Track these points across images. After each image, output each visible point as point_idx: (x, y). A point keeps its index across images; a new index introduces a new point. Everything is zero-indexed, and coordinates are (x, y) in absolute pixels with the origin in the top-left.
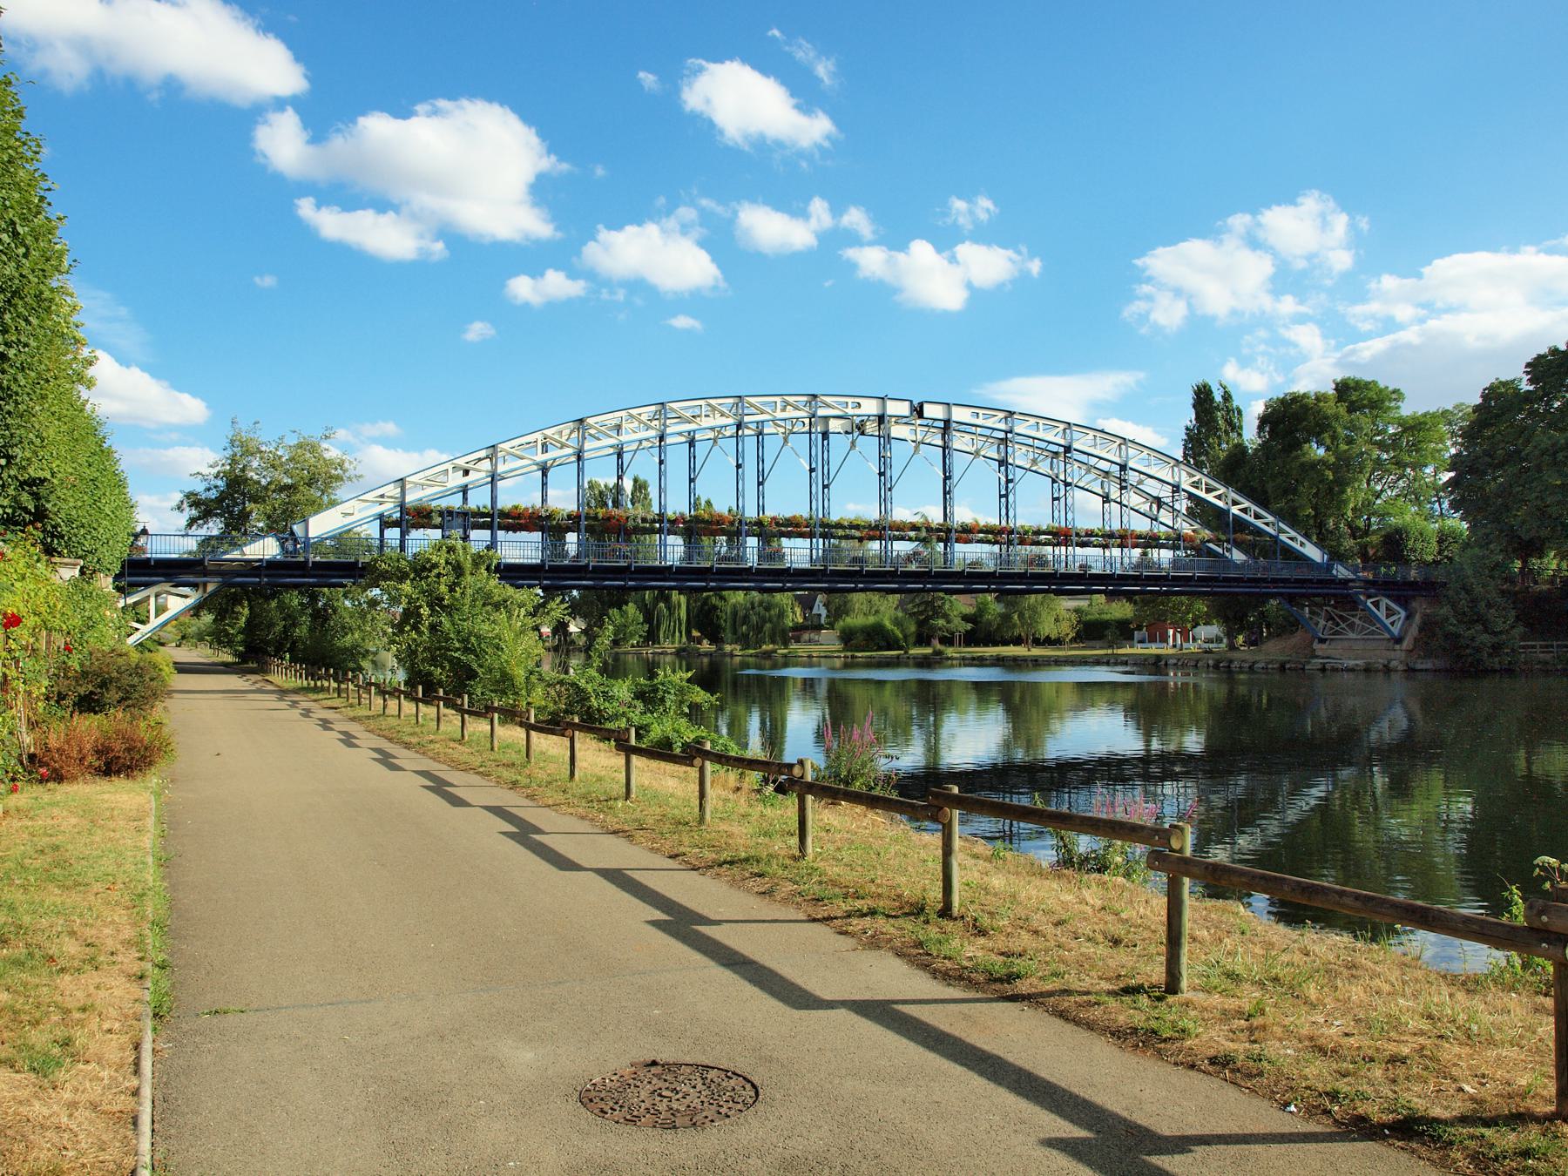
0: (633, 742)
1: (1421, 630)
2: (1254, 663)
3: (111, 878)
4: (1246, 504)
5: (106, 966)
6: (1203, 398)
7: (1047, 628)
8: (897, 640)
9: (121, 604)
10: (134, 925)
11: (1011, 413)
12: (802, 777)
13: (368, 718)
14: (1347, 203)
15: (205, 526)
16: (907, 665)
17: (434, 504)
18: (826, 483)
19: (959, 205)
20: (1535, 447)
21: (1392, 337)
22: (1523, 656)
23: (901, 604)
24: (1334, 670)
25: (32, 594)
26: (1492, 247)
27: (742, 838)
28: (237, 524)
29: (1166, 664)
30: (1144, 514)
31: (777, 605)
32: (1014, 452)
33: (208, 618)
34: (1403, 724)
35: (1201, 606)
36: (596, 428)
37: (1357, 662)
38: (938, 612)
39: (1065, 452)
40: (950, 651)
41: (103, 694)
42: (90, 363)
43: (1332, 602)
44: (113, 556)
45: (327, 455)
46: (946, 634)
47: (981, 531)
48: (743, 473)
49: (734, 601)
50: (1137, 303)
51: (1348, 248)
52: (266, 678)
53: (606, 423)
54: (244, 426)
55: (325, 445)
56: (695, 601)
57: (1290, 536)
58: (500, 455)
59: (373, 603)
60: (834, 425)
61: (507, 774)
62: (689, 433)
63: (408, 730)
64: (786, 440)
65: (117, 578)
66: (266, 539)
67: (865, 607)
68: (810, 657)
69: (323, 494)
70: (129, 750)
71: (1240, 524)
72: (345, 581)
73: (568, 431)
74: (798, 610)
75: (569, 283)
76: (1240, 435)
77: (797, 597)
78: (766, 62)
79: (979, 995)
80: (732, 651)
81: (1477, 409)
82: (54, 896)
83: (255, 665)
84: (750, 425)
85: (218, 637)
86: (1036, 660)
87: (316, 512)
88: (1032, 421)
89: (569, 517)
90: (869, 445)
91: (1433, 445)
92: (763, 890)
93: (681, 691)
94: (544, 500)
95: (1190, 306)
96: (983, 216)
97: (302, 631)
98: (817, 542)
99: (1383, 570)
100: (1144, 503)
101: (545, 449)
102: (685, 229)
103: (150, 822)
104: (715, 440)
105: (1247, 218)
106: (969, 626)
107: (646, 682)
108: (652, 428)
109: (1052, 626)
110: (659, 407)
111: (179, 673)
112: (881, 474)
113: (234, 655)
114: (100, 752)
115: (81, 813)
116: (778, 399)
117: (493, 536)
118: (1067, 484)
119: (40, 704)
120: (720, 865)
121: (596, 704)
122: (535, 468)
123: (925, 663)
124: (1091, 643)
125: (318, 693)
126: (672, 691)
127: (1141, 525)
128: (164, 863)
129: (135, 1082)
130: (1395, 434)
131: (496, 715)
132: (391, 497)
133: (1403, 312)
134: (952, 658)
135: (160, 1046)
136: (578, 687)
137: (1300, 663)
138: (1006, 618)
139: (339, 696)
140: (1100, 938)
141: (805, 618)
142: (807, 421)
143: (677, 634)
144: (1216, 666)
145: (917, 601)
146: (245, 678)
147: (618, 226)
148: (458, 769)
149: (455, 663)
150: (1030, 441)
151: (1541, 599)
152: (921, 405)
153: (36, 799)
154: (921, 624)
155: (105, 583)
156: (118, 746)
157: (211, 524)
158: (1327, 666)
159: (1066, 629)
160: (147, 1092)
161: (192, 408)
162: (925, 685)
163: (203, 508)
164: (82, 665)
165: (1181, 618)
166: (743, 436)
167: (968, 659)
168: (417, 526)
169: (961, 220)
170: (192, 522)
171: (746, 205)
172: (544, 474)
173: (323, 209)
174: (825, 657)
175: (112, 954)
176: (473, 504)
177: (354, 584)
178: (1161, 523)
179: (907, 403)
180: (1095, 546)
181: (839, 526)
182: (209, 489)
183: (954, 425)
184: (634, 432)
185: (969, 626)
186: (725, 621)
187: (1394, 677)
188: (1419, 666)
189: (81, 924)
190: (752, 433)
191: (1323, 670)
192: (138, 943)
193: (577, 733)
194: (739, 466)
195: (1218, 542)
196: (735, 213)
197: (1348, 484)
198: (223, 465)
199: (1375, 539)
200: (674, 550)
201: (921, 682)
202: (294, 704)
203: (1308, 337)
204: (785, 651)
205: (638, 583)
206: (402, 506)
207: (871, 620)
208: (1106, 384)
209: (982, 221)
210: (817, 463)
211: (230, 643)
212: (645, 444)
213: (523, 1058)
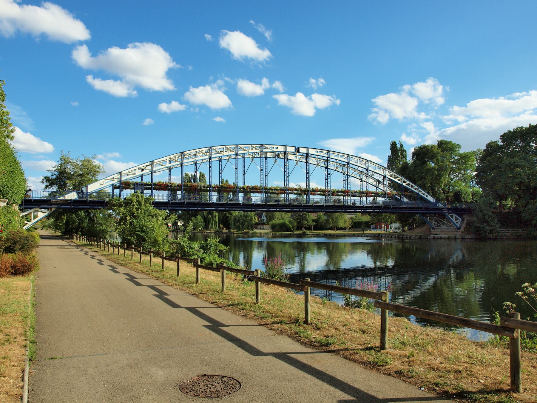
0: (199, 263)
2: (411, 236)
3: (15, 311)
4: (408, 182)
5: (13, 343)
6: (394, 146)
7: (341, 224)
8: (290, 228)
9: (21, 215)
10: (23, 328)
11: (329, 151)
12: (257, 276)
13: (108, 255)
15: (51, 188)
16: (294, 237)
17: (131, 181)
18: (266, 174)
19: (313, 81)
20: (504, 164)
21: (457, 126)
23: (292, 216)
24: (438, 238)
27: (236, 297)
28: (62, 187)
29: (381, 237)
34: (460, 257)
35: (393, 217)
36: (187, 155)
38: (304, 219)
39: (347, 164)
42: (12, 131)
43: (437, 216)
44: (19, 198)
45: (94, 164)
47: (319, 191)
48: (238, 171)
49: (235, 214)
51: (443, 97)
52: (72, 241)
54: (65, 153)
57: (423, 193)
58: (154, 164)
59: (110, 215)
60: (269, 155)
61: (156, 274)
62: (220, 157)
63: (122, 259)
64: (252, 160)
65: (20, 206)
66: (73, 193)
67: (279, 217)
68: (261, 234)
69: (93, 176)
70: (23, 266)
71: (406, 189)
72: (100, 207)
73: (178, 156)
74: (257, 218)
78: (249, 32)
79: (317, 351)
80: (234, 232)
83: (69, 236)
84: (240, 155)
85: (56, 227)
86: (337, 235)
87: (90, 184)
88: (336, 154)
89: (178, 186)
92: (243, 314)
93: (216, 246)
94: (169, 180)
97: (85, 225)
98: (263, 195)
99: (454, 205)
100: (374, 182)
101: (170, 162)
102: (220, 88)
103: (30, 291)
106: (315, 224)
108: (207, 155)
112: (285, 172)
113: (62, 232)
114: (13, 266)
116: (250, 146)
117: (152, 192)
120: (229, 306)
121: (187, 250)
122: (166, 169)
123: (300, 236)
124: (356, 229)
125: (90, 246)
126: (213, 246)
127: (373, 189)
128: (34, 306)
129: (22, 384)
131: (152, 254)
132: (116, 178)
133: (461, 118)
134: (309, 235)
136: (181, 244)
138: (327, 221)
139: (98, 247)
140: (358, 331)
141: (259, 220)
142: (260, 153)
145: (297, 215)
146: (65, 241)
148: (138, 273)
149: (139, 236)
150: (335, 161)
152: (299, 148)
154: (298, 223)
156: (19, 265)
157: (53, 187)
159: (348, 225)
160: (26, 387)
163: (50, 182)
164: (7, 236)
165: (387, 221)
166: (238, 158)
167: (314, 235)
168: (125, 189)
169: (313, 86)
170: (47, 187)
171: (240, 80)
172: (170, 171)
174: (266, 234)
175: (15, 338)
176: (145, 181)
178: (380, 189)
181: (270, 189)
182: (52, 175)
183: (310, 155)
184: (201, 157)
185: (315, 224)
186: (232, 221)
188: (466, 237)
189: (4, 328)
191: (434, 238)
192: (25, 334)
194: (236, 169)
196: (237, 83)
198: (58, 167)
199: (451, 194)
200: (214, 197)
201: (298, 243)
202: (82, 250)
203: (429, 126)
204: (252, 232)
206: (120, 182)
207: (282, 221)
211: (60, 229)
212: (204, 161)
213: (159, 374)
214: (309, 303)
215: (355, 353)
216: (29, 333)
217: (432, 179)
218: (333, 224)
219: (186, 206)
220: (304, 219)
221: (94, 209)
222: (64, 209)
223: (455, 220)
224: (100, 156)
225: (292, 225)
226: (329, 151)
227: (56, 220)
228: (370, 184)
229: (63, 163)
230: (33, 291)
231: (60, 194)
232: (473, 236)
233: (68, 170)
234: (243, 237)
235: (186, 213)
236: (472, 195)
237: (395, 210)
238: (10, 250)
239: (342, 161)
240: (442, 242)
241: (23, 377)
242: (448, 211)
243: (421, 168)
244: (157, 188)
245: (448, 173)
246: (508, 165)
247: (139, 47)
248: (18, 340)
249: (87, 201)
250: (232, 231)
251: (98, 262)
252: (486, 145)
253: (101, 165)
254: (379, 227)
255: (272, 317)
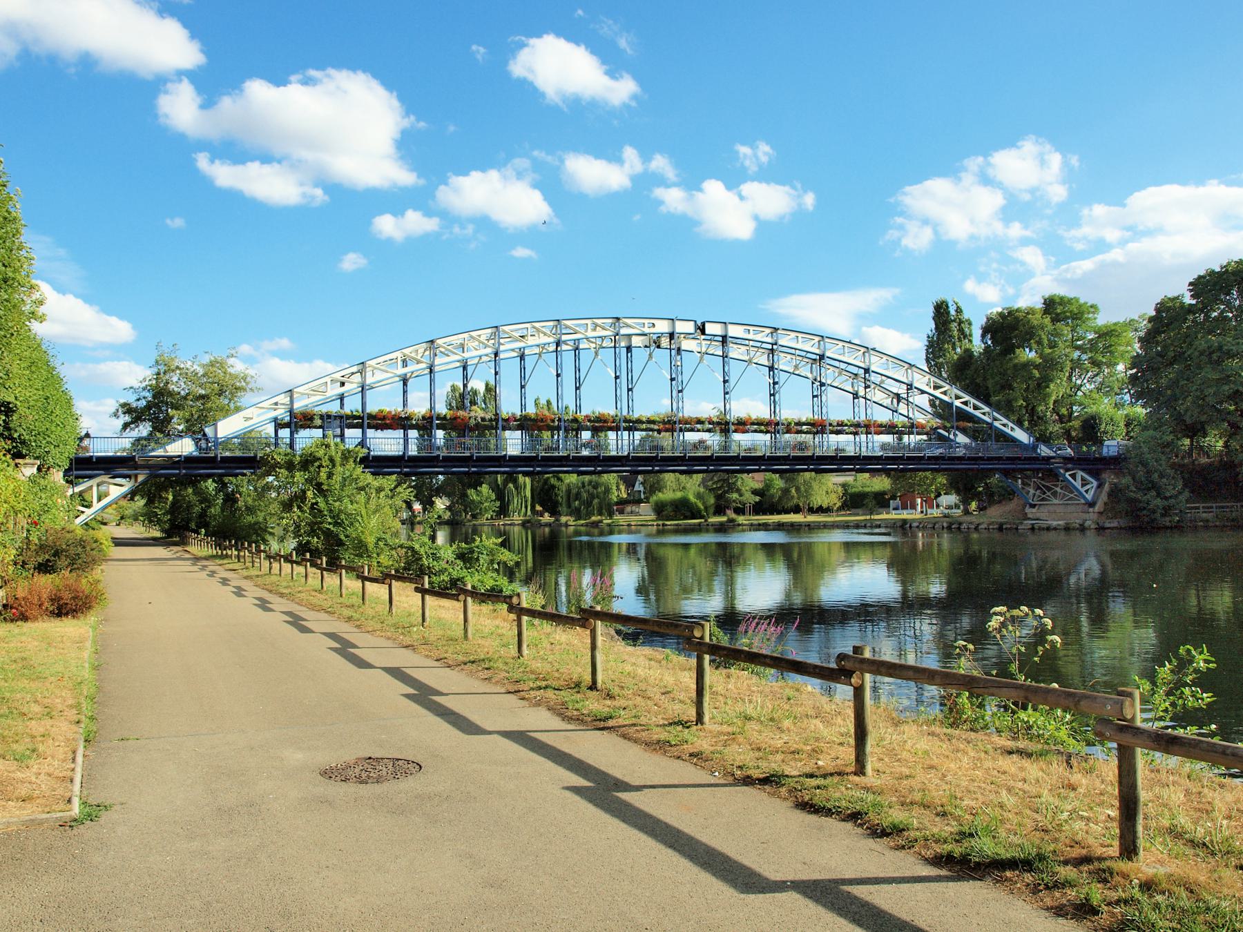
1: (1109, 495)
2: (978, 525)
4: (967, 398)
6: (941, 311)
7: (819, 499)
8: (699, 511)
9: (70, 492)
11: (776, 329)
13: (257, 576)
14: (1061, 147)
15: (137, 429)
16: (707, 531)
17: (317, 409)
18: (630, 387)
19: (744, 150)
20: (1195, 349)
21: (1100, 257)
22: (1189, 515)
23: (704, 482)
24: (1041, 529)
25: (4, 489)
26: (1183, 182)
27: (488, 647)
28: (161, 427)
29: (910, 527)
30: (886, 407)
31: (603, 484)
32: (778, 360)
33: (140, 502)
34: (1096, 571)
35: (942, 480)
36: (444, 348)
37: (1060, 522)
38: (732, 488)
39: (820, 360)
40: (741, 519)
41: (56, 561)
43: (1040, 475)
44: (62, 456)
45: (230, 370)
46: (739, 505)
47: (753, 424)
48: (562, 381)
49: (568, 481)
50: (891, 232)
51: (1063, 182)
53: (453, 342)
55: (231, 361)
56: (538, 482)
57: (1003, 423)
58: (368, 369)
59: (268, 487)
60: (636, 341)
61: (347, 612)
62: (520, 349)
63: (285, 584)
64: (596, 353)
65: (67, 473)
66: (184, 440)
69: (230, 400)
70: (74, 598)
71: (963, 416)
72: (245, 471)
74: (622, 487)
75: (425, 220)
76: (970, 341)
77: (622, 478)
78: (574, 35)
79: (584, 728)
80: (567, 522)
81: (1151, 320)
82: (24, 683)
84: (568, 342)
85: (150, 517)
86: (809, 525)
87: (225, 417)
88: (793, 335)
89: (424, 418)
90: (662, 356)
91: (1122, 348)
93: (491, 553)
94: (405, 404)
95: (936, 232)
96: (764, 159)
98: (622, 434)
99: (1085, 449)
100: (886, 398)
102: (520, 175)
103: (88, 644)
104: (540, 355)
105: (980, 159)
106: (757, 499)
107: (466, 546)
108: (489, 347)
109: (824, 498)
110: (494, 330)
111: (116, 546)
112: (672, 379)
113: (162, 531)
115: (41, 639)
117: (364, 433)
118: (822, 385)
119: (10, 567)
120: (465, 664)
121: (426, 563)
122: (398, 379)
123: (721, 529)
124: (853, 511)
125: (223, 559)
126: (485, 552)
127: (883, 416)
128: (96, 668)
129: (73, 766)
130: (1092, 340)
132: (283, 404)
133: (1112, 235)
134: (742, 525)
135: (88, 753)
137: (1014, 524)
138: (786, 491)
139: (239, 561)
141: (628, 494)
142: (613, 338)
143: (523, 509)
144: (949, 528)
145: (716, 479)
146: (169, 549)
147: (465, 173)
148: (313, 610)
149: (328, 534)
150: (793, 351)
151: (1203, 472)
152: (703, 324)
153: (10, 631)
154: (718, 497)
155: (57, 476)
156: (67, 596)
157: (141, 427)
158: (1036, 526)
159: (834, 500)
160: (79, 770)
161: (120, 330)
162: (722, 546)
163: (135, 415)
164: (40, 539)
165: (926, 490)
166: (561, 351)
167: (755, 525)
168: (304, 427)
169: (747, 163)
170: (126, 426)
171: (571, 155)
172: (405, 384)
173: (217, 162)
174: (641, 525)
176: (347, 410)
177: (252, 473)
178: (900, 414)
179: (692, 323)
180: (847, 433)
181: (639, 421)
182: (138, 400)
183: (730, 339)
184: (476, 349)
185: (757, 499)
187: (1088, 533)
188: (1107, 525)
190: (570, 348)
191: (1033, 529)
192: (77, 706)
193: (393, 581)
194: (558, 375)
195: (945, 428)
196: (562, 161)
197: (1051, 381)
198: (150, 380)
199: (1076, 424)
200: (513, 444)
201: (719, 544)
203: (1032, 257)
204: (610, 521)
205: (479, 469)
206: (291, 411)
207: (679, 495)
208: (869, 299)
209: (764, 163)
210: (620, 371)
211: (159, 522)
212: (484, 359)
213: (296, 757)
214: (597, 650)
215: (643, 731)
216: (86, 706)
217: (1028, 388)
218: (799, 498)
219: (444, 464)
220: (732, 489)
221: (236, 475)
222: (167, 477)
223: (1083, 485)
224: (245, 349)
225: (704, 503)
226: (775, 328)
227: (150, 502)
228: (874, 402)
229: (162, 371)
230: (95, 642)
231: (157, 442)
232: (1123, 522)
233: (173, 386)
234: (588, 534)
235: (455, 478)
236: (1126, 425)
237: (935, 464)
238: (46, 568)
239: (808, 352)
240: (1052, 536)
241: (74, 760)
242: (1065, 464)
243: (1001, 363)
244: (377, 424)
245: (1067, 374)
246: (1204, 350)
247: (321, 81)
248: (66, 713)
249: (216, 457)
250: (564, 519)
251: (233, 592)
252: (1154, 306)
253: (251, 372)
254: (908, 504)
255: (537, 679)
